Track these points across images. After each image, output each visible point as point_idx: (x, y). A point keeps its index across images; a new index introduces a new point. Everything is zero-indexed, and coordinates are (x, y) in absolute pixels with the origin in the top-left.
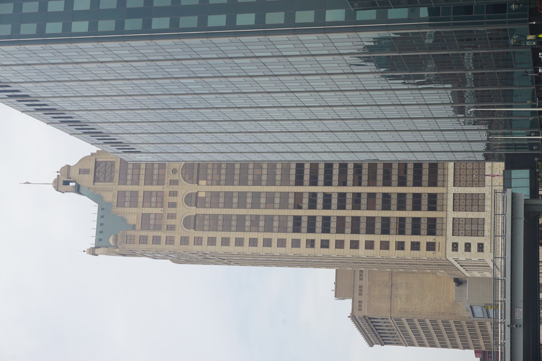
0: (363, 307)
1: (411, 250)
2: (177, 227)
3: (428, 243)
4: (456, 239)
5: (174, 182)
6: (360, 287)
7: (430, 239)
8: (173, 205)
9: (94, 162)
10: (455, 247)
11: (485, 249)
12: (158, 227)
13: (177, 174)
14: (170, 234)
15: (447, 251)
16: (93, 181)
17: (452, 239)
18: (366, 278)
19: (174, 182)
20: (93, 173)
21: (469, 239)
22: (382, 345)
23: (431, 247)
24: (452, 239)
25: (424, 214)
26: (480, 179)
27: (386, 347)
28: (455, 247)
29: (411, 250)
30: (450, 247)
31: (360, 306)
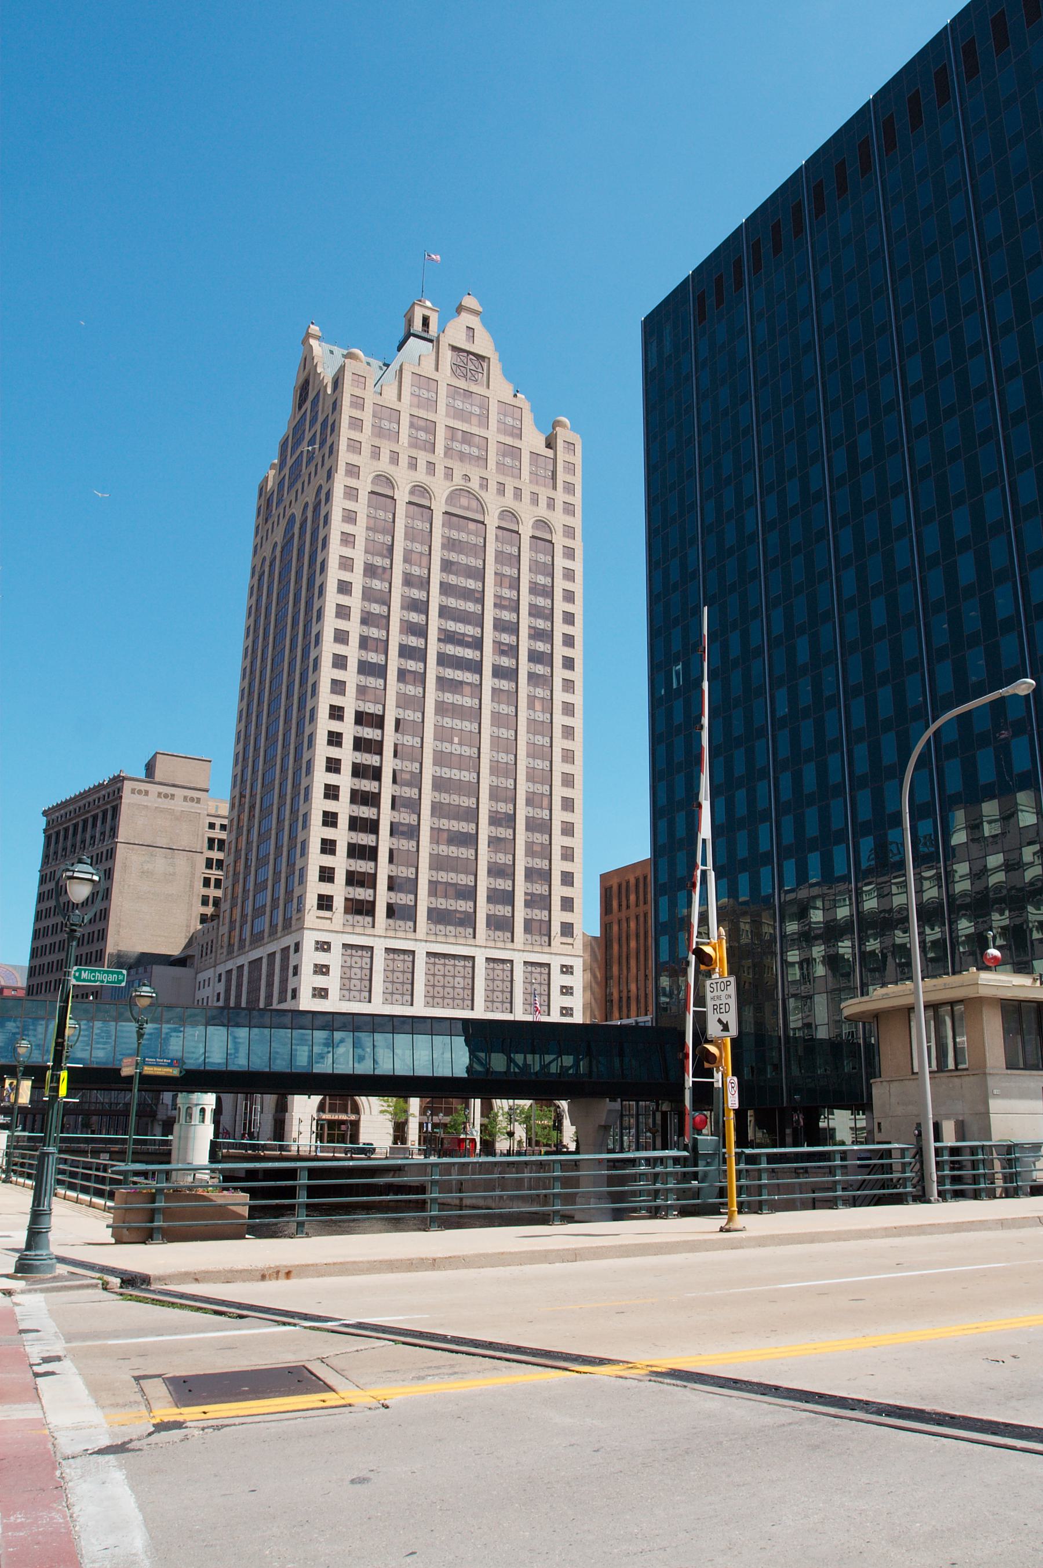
0: (136, 796)
1: (321, 867)
2: (375, 463)
3: (330, 898)
4: (337, 949)
5: (449, 473)
6: (173, 795)
7: (339, 903)
8: (413, 465)
9: (484, 354)
10: (323, 947)
11: (317, 1000)
12: (379, 432)
13: (462, 482)
14: (366, 449)
15: (315, 932)
16: (455, 344)
17: (337, 942)
18: (188, 806)
19: (449, 473)
20: (468, 349)
21: (335, 972)
22: (45, 831)
23: (325, 903)
24: (337, 942)
25: (383, 897)
26: (495, 1004)
27: (41, 839)
28: (323, 947)
29: (321, 867)
30: (324, 937)
31: (140, 792)
